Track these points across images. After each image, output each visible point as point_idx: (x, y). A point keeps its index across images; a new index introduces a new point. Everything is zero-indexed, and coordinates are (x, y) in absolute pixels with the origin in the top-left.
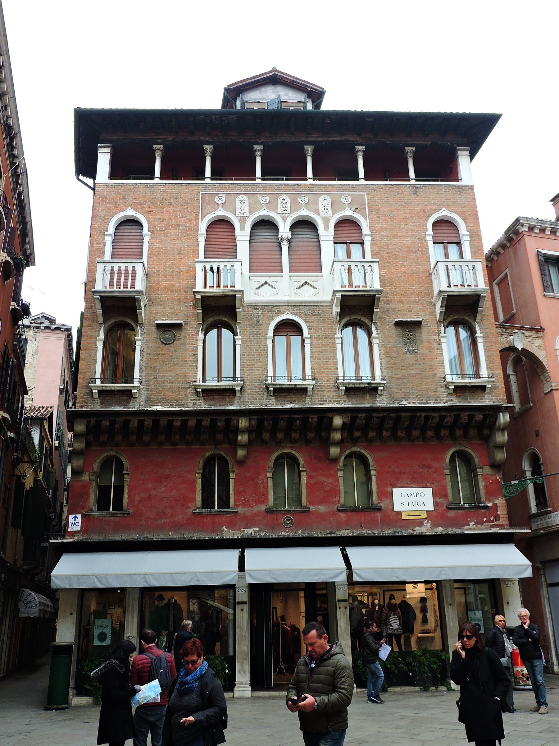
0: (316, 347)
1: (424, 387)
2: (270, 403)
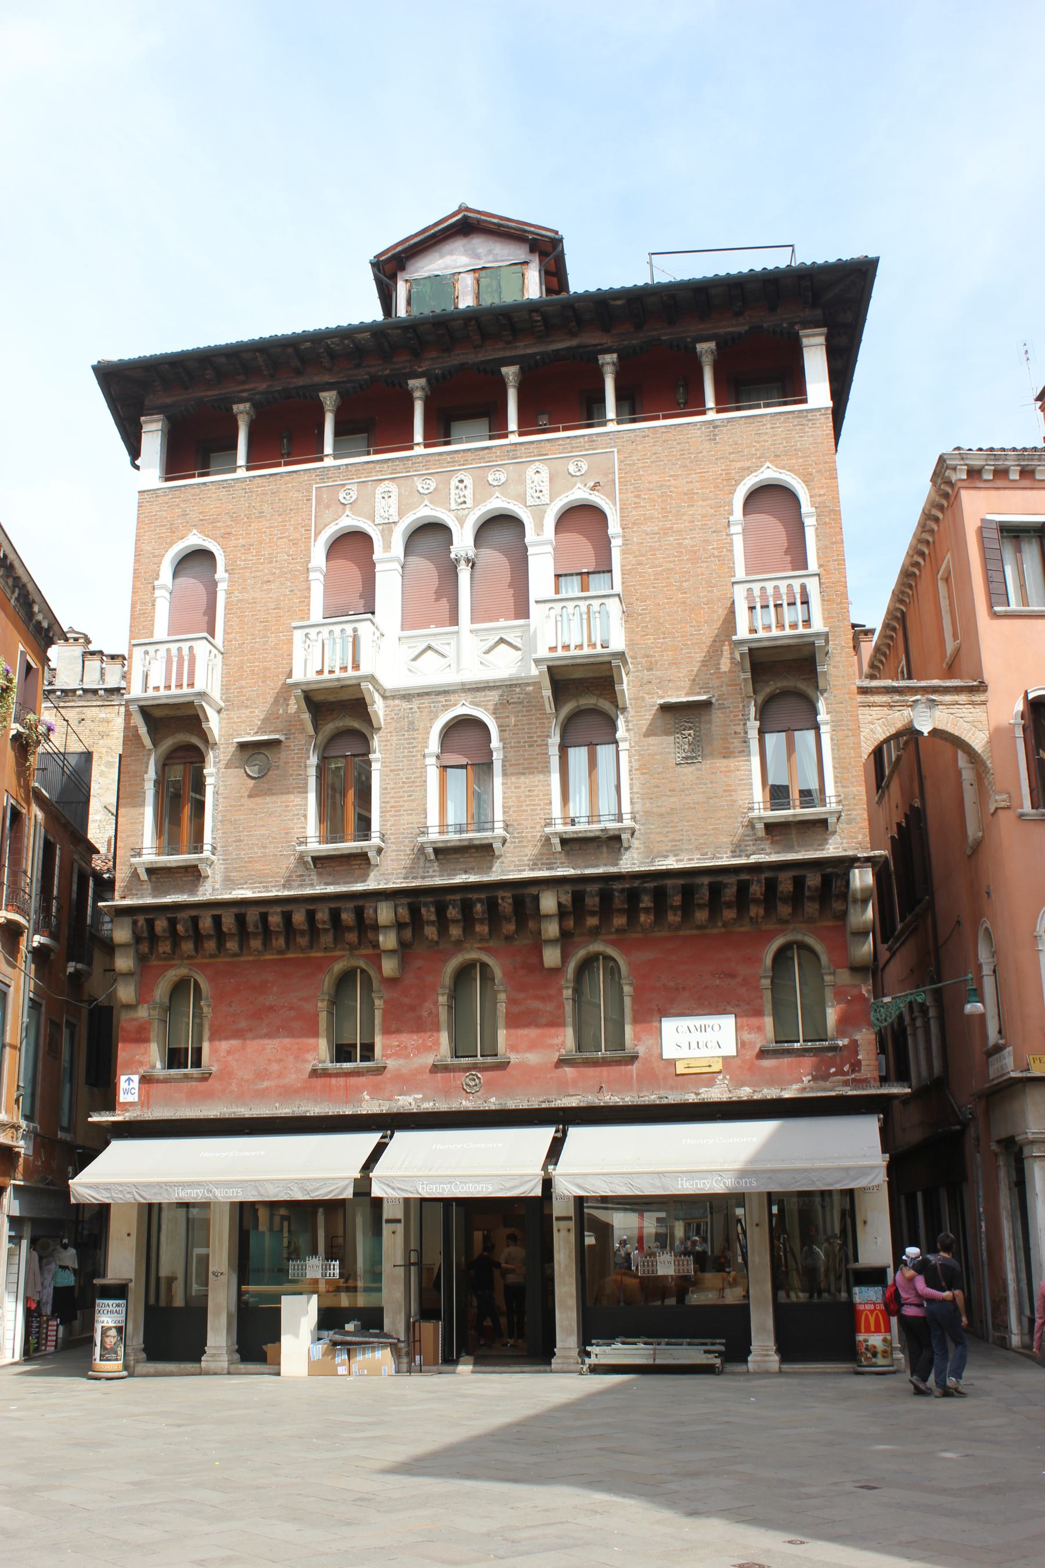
0: (511, 765)
1: (710, 827)
2: (430, 874)
